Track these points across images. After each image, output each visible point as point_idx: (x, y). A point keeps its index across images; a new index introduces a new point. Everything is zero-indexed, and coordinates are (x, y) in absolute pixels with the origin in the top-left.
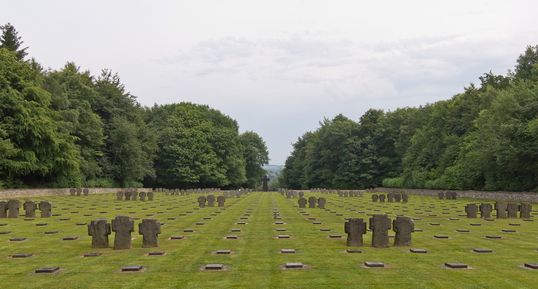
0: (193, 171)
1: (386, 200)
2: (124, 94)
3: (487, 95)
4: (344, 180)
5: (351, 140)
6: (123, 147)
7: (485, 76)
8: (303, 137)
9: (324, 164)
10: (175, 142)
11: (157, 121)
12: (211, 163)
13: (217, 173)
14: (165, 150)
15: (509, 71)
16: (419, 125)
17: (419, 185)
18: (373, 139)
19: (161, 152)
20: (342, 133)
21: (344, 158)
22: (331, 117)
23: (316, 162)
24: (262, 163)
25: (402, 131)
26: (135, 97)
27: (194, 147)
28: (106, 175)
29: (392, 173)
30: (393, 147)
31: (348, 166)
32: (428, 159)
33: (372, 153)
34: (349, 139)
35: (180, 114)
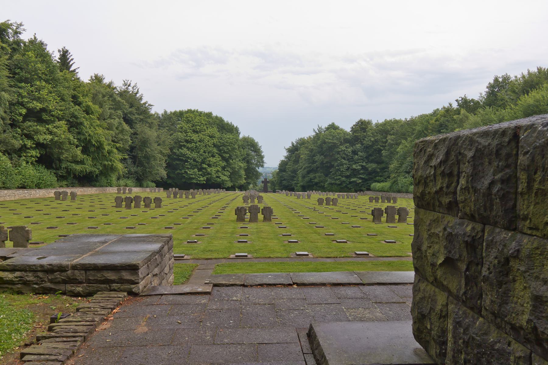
0: (200, 173)
1: (380, 201)
2: (142, 102)
3: (461, 117)
4: (336, 184)
6: (146, 151)
7: (461, 99)
9: (317, 168)
10: (184, 146)
13: (221, 175)
15: (481, 94)
16: (404, 136)
17: (404, 190)
18: (363, 147)
20: (335, 141)
21: (336, 164)
22: (324, 125)
25: (389, 141)
26: (151, 106)
28: (130, 176)
30: (381, 155)
32: (412, 167)
33: (362, 159)
34: (341, 147)
35: (189, 120)
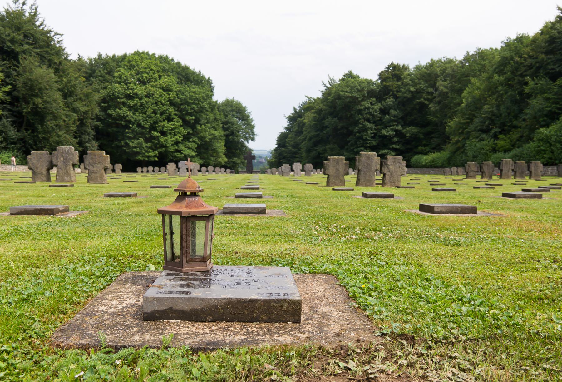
0: (149, 145)
5: (366, 104)
6: (34, 104)
8: (299, 107)
10: (124, 104)
11: (101, 76)
12: (175, 135)
14: (110, 116)
19: (105, 119)
20: (355, 94)
22: (338, 77)
23: (318, 135)
24: (246, 139)
27: (150, 111)
29: (423, 148)
31: (362, 139)
34: (364, 103)
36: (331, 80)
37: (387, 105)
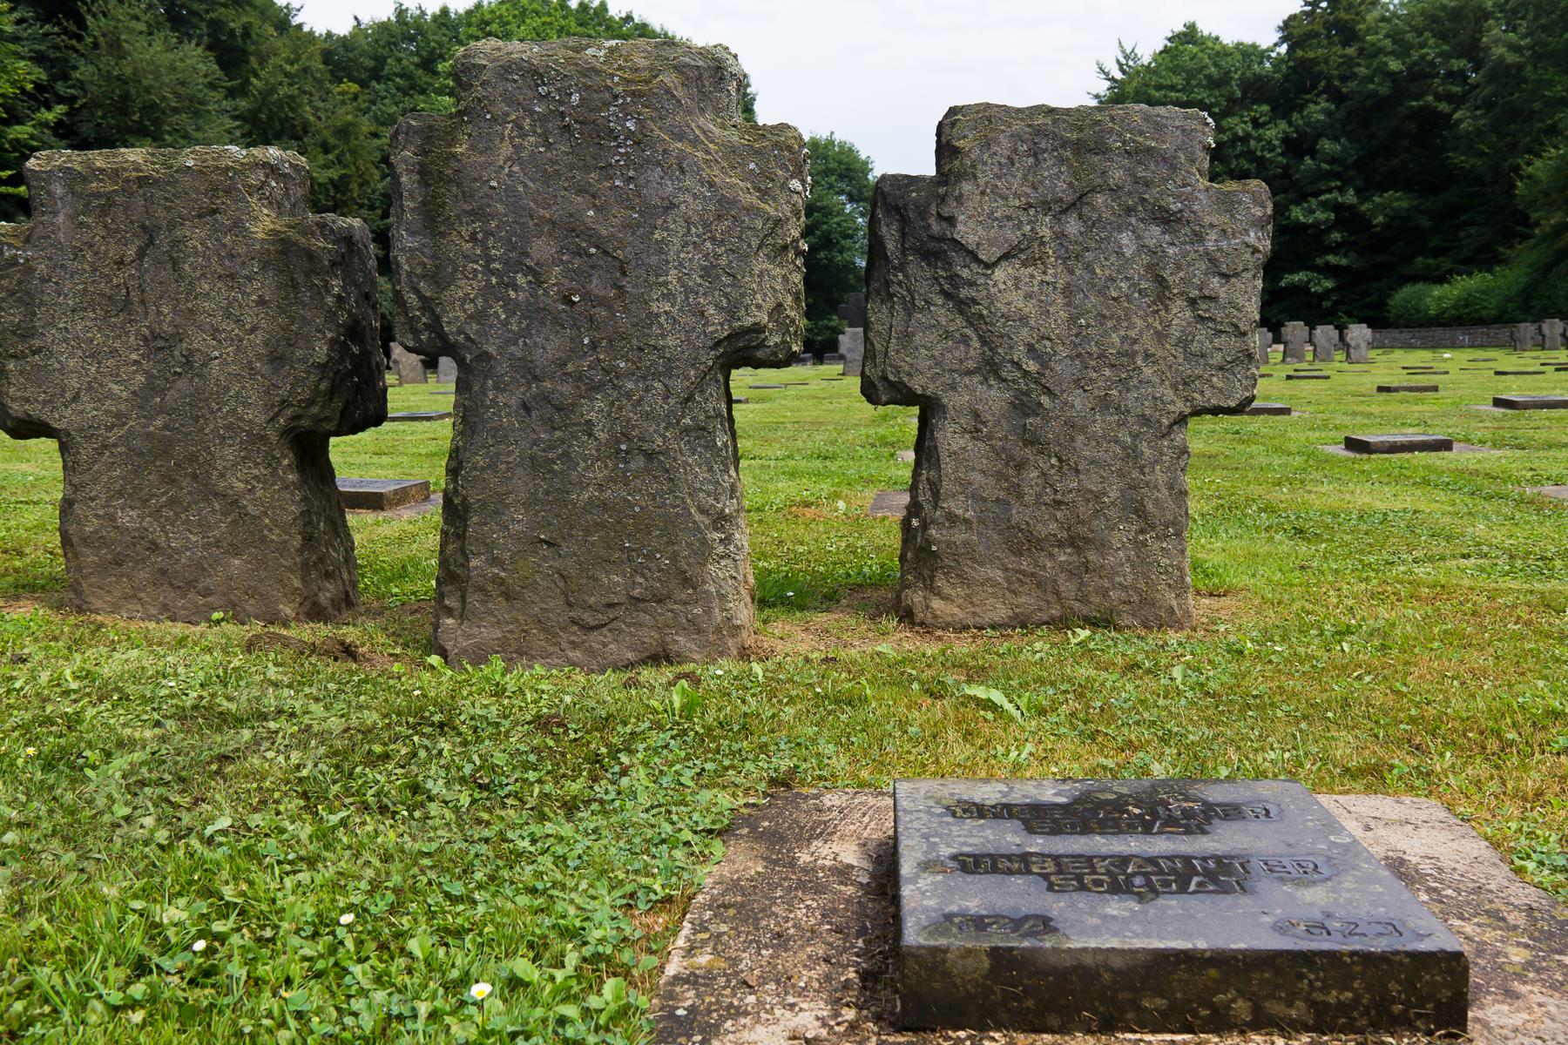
29: (1431, 261)
36: (1127, 57)
37: (1308, 124)
